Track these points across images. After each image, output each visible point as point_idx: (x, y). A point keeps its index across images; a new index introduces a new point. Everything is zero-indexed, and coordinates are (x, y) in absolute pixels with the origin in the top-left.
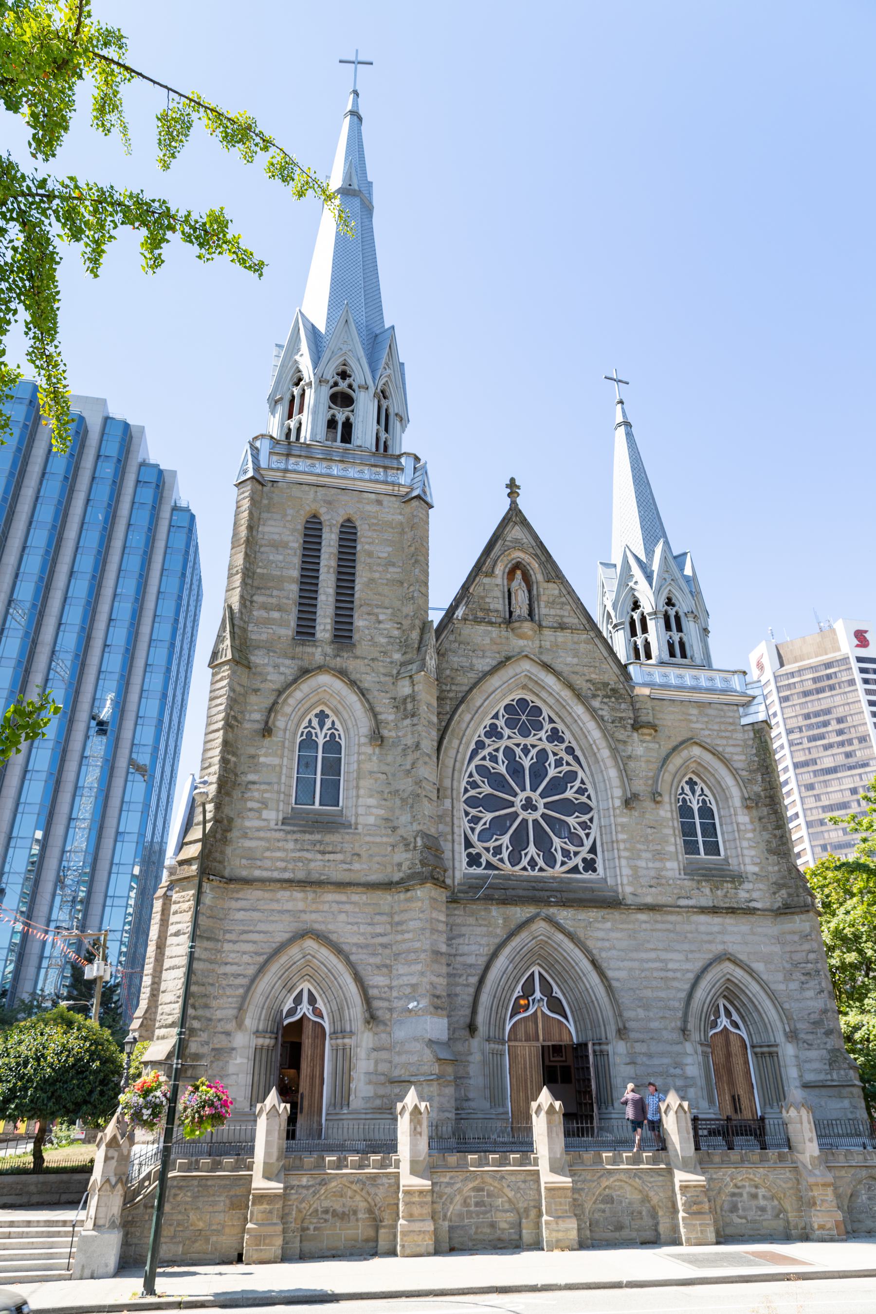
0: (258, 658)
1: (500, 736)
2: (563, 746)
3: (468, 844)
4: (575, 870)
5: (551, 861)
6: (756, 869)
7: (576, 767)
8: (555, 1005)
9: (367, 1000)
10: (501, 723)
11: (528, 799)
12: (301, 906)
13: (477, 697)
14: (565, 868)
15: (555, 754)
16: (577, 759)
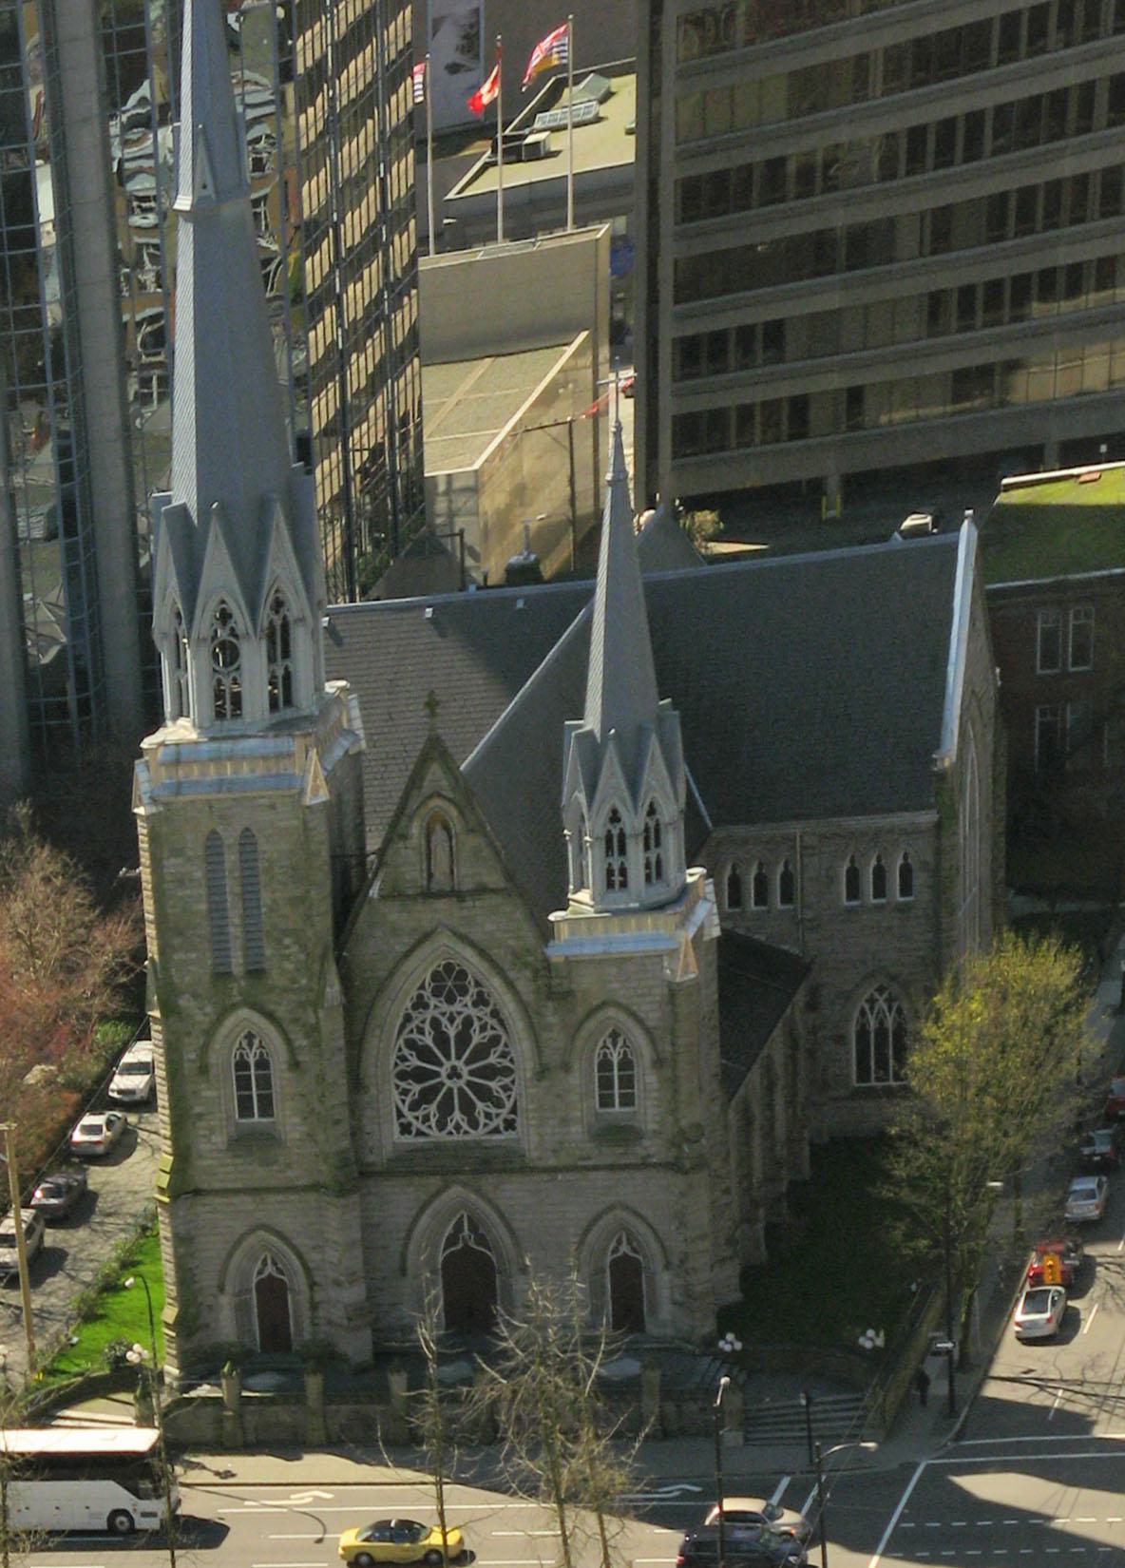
0: (185, 1002)
1: (426, 1006)
2: (488, 1010)
3: (400, 1115)
4: (496, 1131)
5: (474, 1124)
6: (655, 1127)
7: (500, 1031)
8: (481, 1240)
9: (307, 1270)
10: (427, 993)
11: (454, 1068)
12: (251, 1207)
13: (398, 981)
14: (487, 1129)
15: (480, 1019)
16: (501, 1022)
